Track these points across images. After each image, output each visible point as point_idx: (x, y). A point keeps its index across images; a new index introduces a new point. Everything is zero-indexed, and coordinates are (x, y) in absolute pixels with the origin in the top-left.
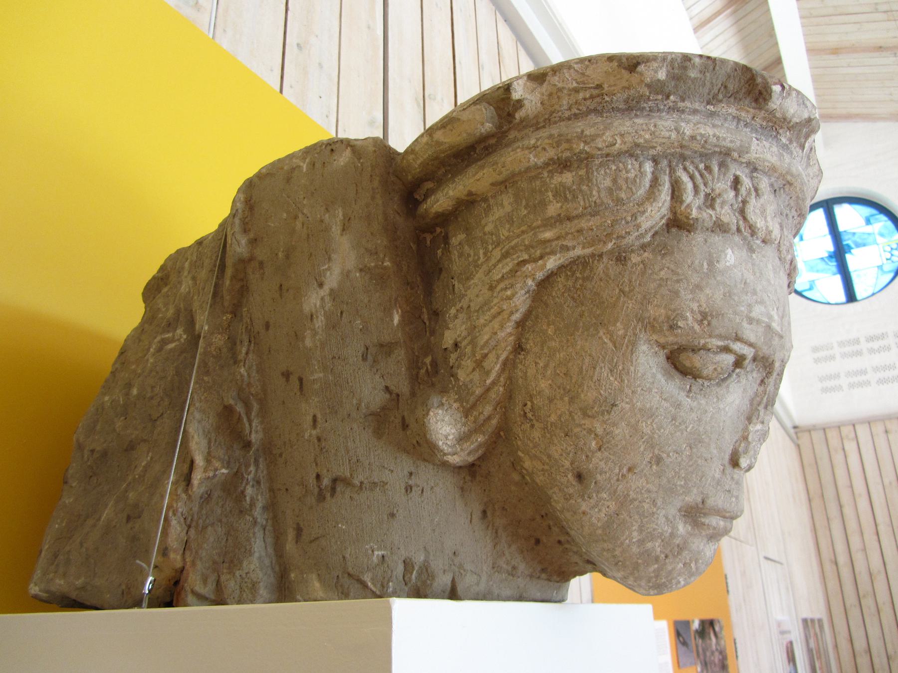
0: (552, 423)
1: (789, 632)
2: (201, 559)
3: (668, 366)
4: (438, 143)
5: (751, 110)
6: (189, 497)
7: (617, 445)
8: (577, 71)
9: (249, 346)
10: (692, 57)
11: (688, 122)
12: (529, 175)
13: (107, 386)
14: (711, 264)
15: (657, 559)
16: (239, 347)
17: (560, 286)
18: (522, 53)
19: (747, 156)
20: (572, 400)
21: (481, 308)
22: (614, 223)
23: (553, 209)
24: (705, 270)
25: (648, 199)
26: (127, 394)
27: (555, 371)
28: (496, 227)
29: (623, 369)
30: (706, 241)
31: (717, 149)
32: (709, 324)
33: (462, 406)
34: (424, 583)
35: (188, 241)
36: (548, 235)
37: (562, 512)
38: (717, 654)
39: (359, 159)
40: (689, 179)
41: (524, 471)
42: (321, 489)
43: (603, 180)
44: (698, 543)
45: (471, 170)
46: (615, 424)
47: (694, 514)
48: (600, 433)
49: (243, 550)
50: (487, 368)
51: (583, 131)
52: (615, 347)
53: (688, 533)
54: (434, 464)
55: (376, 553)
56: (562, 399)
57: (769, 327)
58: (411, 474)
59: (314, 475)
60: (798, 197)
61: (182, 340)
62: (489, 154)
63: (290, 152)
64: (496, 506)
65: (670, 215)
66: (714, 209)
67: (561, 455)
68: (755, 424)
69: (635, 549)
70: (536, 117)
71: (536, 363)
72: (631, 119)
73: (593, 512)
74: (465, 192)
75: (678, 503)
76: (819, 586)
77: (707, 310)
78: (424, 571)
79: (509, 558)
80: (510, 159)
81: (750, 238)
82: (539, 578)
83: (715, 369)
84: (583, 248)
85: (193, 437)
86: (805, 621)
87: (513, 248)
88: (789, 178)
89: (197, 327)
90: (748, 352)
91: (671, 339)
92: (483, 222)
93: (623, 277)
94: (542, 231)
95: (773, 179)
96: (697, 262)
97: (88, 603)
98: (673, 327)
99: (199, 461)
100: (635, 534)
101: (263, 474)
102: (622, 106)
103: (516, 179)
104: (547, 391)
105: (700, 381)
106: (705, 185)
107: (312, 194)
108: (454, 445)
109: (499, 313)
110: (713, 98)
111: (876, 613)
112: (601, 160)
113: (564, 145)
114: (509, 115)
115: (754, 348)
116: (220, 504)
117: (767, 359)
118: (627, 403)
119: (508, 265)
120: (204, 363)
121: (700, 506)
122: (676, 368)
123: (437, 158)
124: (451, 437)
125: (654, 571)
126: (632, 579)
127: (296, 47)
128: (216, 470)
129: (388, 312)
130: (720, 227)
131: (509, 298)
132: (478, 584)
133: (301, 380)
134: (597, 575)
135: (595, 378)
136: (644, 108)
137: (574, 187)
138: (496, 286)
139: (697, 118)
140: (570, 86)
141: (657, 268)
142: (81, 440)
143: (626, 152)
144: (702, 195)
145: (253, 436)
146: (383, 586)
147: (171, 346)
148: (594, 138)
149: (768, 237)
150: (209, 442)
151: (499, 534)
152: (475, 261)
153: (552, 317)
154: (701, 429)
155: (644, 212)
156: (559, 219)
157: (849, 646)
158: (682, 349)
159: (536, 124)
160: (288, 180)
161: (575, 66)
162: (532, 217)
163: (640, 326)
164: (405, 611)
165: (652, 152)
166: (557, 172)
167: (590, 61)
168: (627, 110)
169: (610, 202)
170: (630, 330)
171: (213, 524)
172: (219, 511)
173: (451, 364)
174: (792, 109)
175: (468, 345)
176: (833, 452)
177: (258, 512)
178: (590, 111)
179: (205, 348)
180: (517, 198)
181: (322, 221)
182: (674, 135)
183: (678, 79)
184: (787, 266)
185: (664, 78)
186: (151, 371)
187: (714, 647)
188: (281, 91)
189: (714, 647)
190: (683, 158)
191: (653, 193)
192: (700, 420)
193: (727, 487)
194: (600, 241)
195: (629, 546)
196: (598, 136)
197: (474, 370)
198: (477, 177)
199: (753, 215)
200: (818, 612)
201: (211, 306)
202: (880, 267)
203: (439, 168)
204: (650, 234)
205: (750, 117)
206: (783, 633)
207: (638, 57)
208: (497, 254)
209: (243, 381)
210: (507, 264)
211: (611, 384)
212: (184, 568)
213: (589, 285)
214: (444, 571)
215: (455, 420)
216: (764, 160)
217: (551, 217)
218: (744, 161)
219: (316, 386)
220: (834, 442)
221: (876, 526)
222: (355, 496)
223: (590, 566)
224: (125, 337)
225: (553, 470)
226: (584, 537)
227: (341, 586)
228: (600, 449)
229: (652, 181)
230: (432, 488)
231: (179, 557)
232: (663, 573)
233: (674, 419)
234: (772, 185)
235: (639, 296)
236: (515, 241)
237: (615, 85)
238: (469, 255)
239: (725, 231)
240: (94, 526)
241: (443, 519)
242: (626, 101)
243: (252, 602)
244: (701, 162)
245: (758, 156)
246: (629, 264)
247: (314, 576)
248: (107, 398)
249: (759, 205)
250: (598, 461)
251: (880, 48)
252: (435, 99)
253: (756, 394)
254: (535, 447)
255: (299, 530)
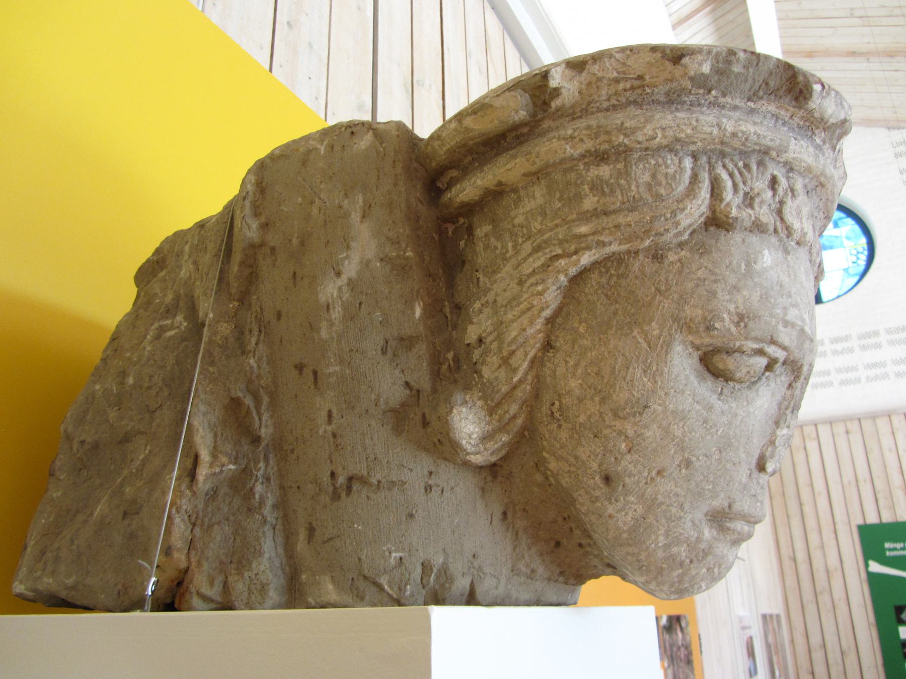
0: (580, 424)
1: (749, 628)
3: (700, 368)
4: (467, 130)
6: (194, 493)
8: (618, 61)
9: (259, 335)
10: (737, 51)
11: (729, 118)
12: (564, 166)
13: (98, 374)
14: (748, 264)
15: (681, 564)
16: (248, 337)
17: (594, 283)
20: (603, 401)
21: (509, 302)
22: (654, 219)
23: (589, 203)
24: (743, 271)
25: (688, 196)
26: (122, 383)
28: (527, 218)
29: (657, 370)
30: (744, 241)
31: (757, 148)
32: (746, 326)
33: (486, 403)
34: (442, 586)
35: (187, 223)
36: (583, 229)
37: (586, 515)
38: (682, 649)
39: (381, 144)
40: (728, 177)
41: (549, 473)
42: (335, 488)
44: (722, 548)
45: (502, 160)
46: (646, 427)
47: (720, 519)
48: (630, 435)
49: (252, 550)
51: (622, 123)
52: (650, 348)
54: (454, 464)
55: (394, 555)
56: (592, 399)
57: (802, 331)
58: (431, 473)
59: (329, 473)
60: (827, 199)
61: (182, 327)
62: (521, 143)
65: (708, 213)
66: (753, 208)
67: (589, 457)
68: (782, 429)
69: (660, 554)
70: (573, 106)
72: (672, 113)
73: (622, 514)
74: (495, 182)
76: (777, 581)
77: (744, 312)
78: (443, 573)
81: (785, 240)
82: (556, 581)
83: (748, 372)
84: (620, 244)
85: (198, 430)
86: (764, 617)
87: (545, 242)
88: (822, 179)
89: (201, 314)
90: (780, 355)
91: (707, 340)
92: (512, 214)
93: (659, 275)
94: (578, 226)
95: (807, 180)
96: (735, 262)
98: (709, 328)
99: (205, 456)
100: (661, 538)
101: (272, 470)
102: (662, 99)
103: (550, 170)
104: (577, 391)
105: (731, 383)
106: (744, 183)
109: (529, 309)
112: (640, 153)
113: (603, 137)
114: (545, 103)
116: (227, 502)
118: (660, 405)
119: (540, 260)
120: (209, 353)
121: (727, 510)
122: (709, 370)
123: (465, 145)
125: (678, 576)
126: (654, 583)
128: (223, 465)
129: (409, 304)
130: (758, 227)
131: (541, 294)
132: (497, 587)
133: (315, 373)
134: (617, 579)
135: (628, 378)
136: (685, 102)
137: (612, 181)
138: (526, 281)
139: (736, 115)
141: (694, 267)
144: (741, 194)
146: (400, 589)
147: (171, 333)
148: (634, 130)
149: (803, 239)
150: (215, 436)
153: (584, 315)
154: (731, 433)
155: (683, 210)
156: (596, 214)
158: (716, 351)
159: (573, 113)
160: (304, 163)
162: (566, 210)
163: (675, 326)
164: (441, 616)
165: (693, 148)
167: (631, 50)
168: (668, 103)
169: (649, 197)
170: (666, 330)
171: (219, 523)
172: (226, 509)
173: (474, 361)
174: (829, 109)
175: (494, 341)
178: (629, 103)
179: (210, 337)
180: (550, 189)
181: (340, 207)
182: (715, 131)
183: (722, 74)
184: (816, 269)
185: (708, 71)
186: (149, 359)
188: (271, 70)
190: (723, 155)
191: (693, 190)
192: (730, 423)
193: (753, 492)
194: (637, 237)
195: (654, 550)
196: (638, 128)
197: (500, 366)
198: (509, 166)
199: (790, 217)
200: (775, 607)
202: (846, 270)
203: (466, 156)
204: (688, 232)
205: (789, 115)
206: (744, 628)
207: (683, 49)
208: (528, 247)
209: (252, 372)
210: (539, 259)
211: (644, 385)
212: (188, 568)
213: (623, 282)
214: (463, 574)
215: (479, 418)
216: (801, 161)
217: (587, 211)
218: (782, 160)
219: (333, 380)
222: (372, 495)
223: (609, 570)
224: (116, 323)
225: (579, 472)
227: (357, 588)
228: (629, 451)
229: (691, 178)
231: (183, 557)
233: (705, 422)
234: (805, 186)
235: (676, 296)
237: (657, 77)
238: (496, 248)
239: (763, 232)
240: (86, 521)
241: (459, 522)
242: (667, 94)
244: (741, 160)
245: (795, 155)
246: (666, 262)
247: (327, 578)
248: (98, 387)
250: (627, 463)
253: (784, 398)
254: (562, 448)
255: (311, 530)
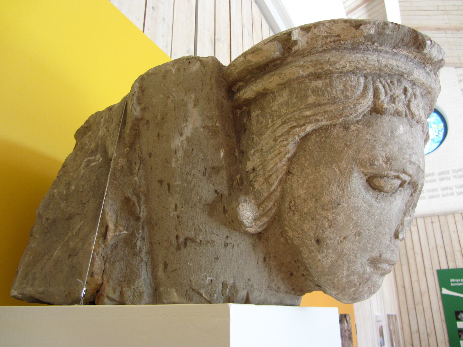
0: (305, 213)
1: (381, 321)
2: (112, 279)
3: (366, 184)
4: (249, 61)
5: (415, 53)
6: (106, 245)
8: (327, 27)
9: (140, 165)
11: (384, 57)
12: (298, 81)
13: (56, 184)
15: (355, 285)
16: (134, 166)
17: (313, 141)
18: (264, 20)
19: (411, 77)
20: (317, 201)
21: (269, 150)
22: (344, 108)
23: (311, 99)
25: (362, 97)
26: (68, 189)
27: (308, 185)
28: (279, 107)
31: (397, 73)
32: (390, 164)
34: (233, 295)
35: (102, 108)
36: (308, 113)
38: (347, 332)
42: (178, 244)
43: (338, 85)
44: (376, 278)
45: (266, 77)
46: (338, 214)
47: (375, 262)
49: (135, 275)
50: (271, 182)
51: (329, 59)
52: (341, 174)
53: (372, 272)
54: (239, 232)
55: (208, 278)
56: (311, 200)
57: (419, 167)
58: (227, 237)
59: (175, 236)
60: (432, 100)
61: (100, 161)
63: (166, 62)
64: (271, 255)
65: (372, 106)
66: (395, 104)
67: (309, 229)
68: (407, 217)
69: (344, 280)
70: (304, 50)
71: (298, 181)
72: (354, 54)
73: (325, 259)
74: (263, 88)
75: (368, 256)
77: (390, 156)
78: (233, 288)
79: (276, 283)
80: (289, 72)
81: (411, 120)
82: (290, 293)
83: (391, 187)
84: (327, 121)
85: (108, 213)
86: (388, 316)
87: (288, 119)
88: (430, 90)
89: (110, 154)
90: (407, 179)
91: (370, 171)
92: (271, 105)
93: (347, 137)
94: (305, 111)
96: (385, 131)
99: (111, 226)
100: (345, 272)
101: (146, 234)
104: (303, 196)
105: (382, 193)
106: (391, 91)
108: (252, 222)
109: (279, 154)
111: (423, 312)
112: (337, 75)
116: (123, 250)
118: (346, 203)
119: (285, 128)
120: (114, 174)
121: (379, 258)
122: (371, 186)
123: (247, 69)
124: (250, 218)
126: (341, 295)
127: (151, 8)
128: (121, 231)
130: (397, 113)
131: (285, 146)
132: (260, 296)
133: (169, 185)
134: (321, 293)
135: (330, 189)
136: (361, 48)
137: (323, 88)
139: (387, 56)
141: (365, 133)
142: (41, 212)
143: (351, 71)
144: (389, 96)
145: (141, 214)
147: (93, 164)
148: (335, 63)
149: (420, 120)
150: (117, 216)
151: (272, 270)
153: (308, 157)
155: (360, 103)
156: (314, 105)
157: (409, 329)
158: (375, 176)
160: (164, 77)
164: (235, 309)
165: (364, 72)
166: (314, 80)
167: (334, 22)
168: (352, 49)
169: (342, 97)
172: (122, 254)
175: (261, 170)
177: (143, 255)
178: (333, 49)
180: (291, 92)
181: (183, 100)
182: (376, 64)
184: (425, 135)
186: (82, 177)
188: (143, 31)
191: (365, 94)
192: (381, 214)
193: (392, 249)
194: (336, 117)
196: (337, 62)
197: (264, 183)
198: (270, 80)
199: (413, 109)
200: (394, 311)
201: (118, 144)
204: (362, 115)
208: (279, 122)
209: (136, 184)
211: (338, 193)
212: (102, 283)
213: (328, 141)
215: (253, 209)
217: (310, 104)
218: (409, 79)
219: (178, 188)
222: (198, 248)
223: (318, 288)
225: (304, 237)
226: (318, 273)
227: (189, 295)
228: (330, 227)
229: (364, 87)
230: (238, 245)
233: (369, 212)
235: (355, 148)
237: (347, 36)
238: (262, 122)
240: (49, 259)
241: (241, 261)
242: (352, 45)
243: (140, 303)
246: (350, 130)
247: (174, 290)
248: (55, 191)
250: (328, 233)
253: (408, 201)
254: (295, 225)
255: (166, 265)
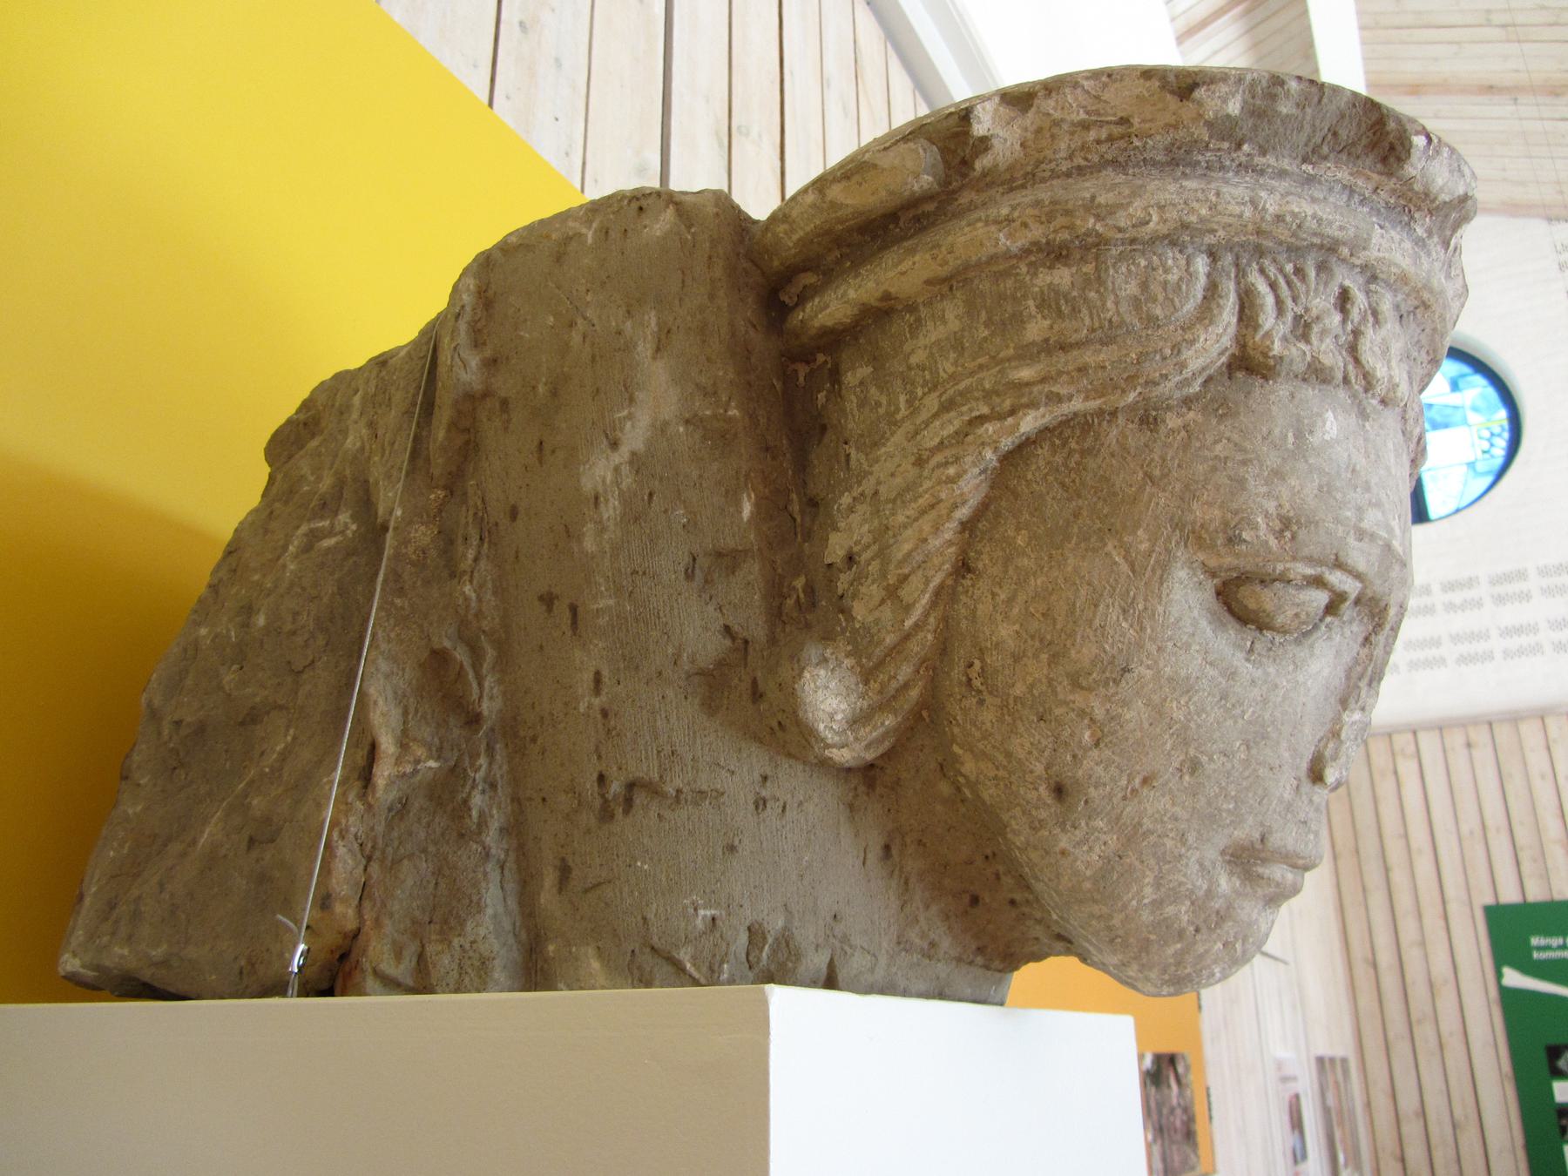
0: (1016, 699)
1: (1294, 1079)
2: (391, 915)
4: (834, 205)
5: (1375, 176)
6: (370, 807)
7: (1127, 739)
9: (480, 546)
11: (1271, 191)
12: (995, 268)
14: (1299, 435)
15: (1181, 934)
16: (461, 549)
17: (1042, 463)
19: (1362, 254)
20: (1054, 659)
23: (1036, 329)
24: (1290, 446)
25: (1200, 319)
26: (246, 625)
28: (931, 355)
30: (1292, 396)
31: (1317, 241)
32: (1293, 538)
33: (859, 663)
35: (356, 359)
36: (1026, 373)
38: (1178, 1112)
39: (689, 227)
40: (1268, 289)
41: (961, 779)
42: (606, 801)
44: (1249, 909)
45: (890, 257)
46: (1125, 703)
47: (1247, 859)
51: (1093, 198)
52: (1134, 571)
54: (804, 763)
55: (702, 912)
57: (1388, 547)
58: (765, 778)
59: (595, 776)
60: (1435, 330)
62: (923, 229)
65: (1234, 350)
66: (1308, 342)
67: (1030, 753)
68: (1352, 711)
69: (1146, 916)
70: (1011, 168)
71: (994, 595)
72: (1175, 180)
73: (1083, 849)
74: (878, 294)
75: (1221, 840)
77: (1291, 514)
79: (925, 928)
81: (1362, 395)
82: (971, 963)
83: (1297, 615)
84: (1087, 398)
85: (375, 703)
86: (1320, 1061)
87: (961, 394)
88: (1426, 295)
90: (1351, 586)
91: (1229, 560)
92: (907, 348)
94: (1016, 368)
95: (1400, 297)
96: (1277, 431)
97: (172, 989)
98: (1233, 540)
99: (387, 744)
100: (1148, 890)
101: (501, 770)
104: (1010, 641)
105: (1268, 634)
107: (603, 284)
109: (932, 506)
110: (1313, 151)
113: (1060, 221)
115: (1362, 581)
117: (1377, 605)
118: (1148, 667)
121: (1258, 846)
122: (1230, 610)
123: (828, 232)
126: (1135, 967)
128: (417, 762)
129: (733, 497)
130: (1317, 373)
132: (872, 970)
133: (574, 609)
134: (1073, 961)
135: (1097, 622)
136: (1198, 162)
137: (1075, 293)
139: (1284, 185)
140: (1075, 117)
141: (1210, 439)
142: (157, 702)
143: (1165, 237)
144: (1289, 317)
148: (1112, 210)
150: (405, 713)
151: (911, 886)
152: (892, 415)
154: (1267, 716)
155: (1193, 342)
156: (1048, 347)
158: (1244, 579)
160: (559, 258)
161: (1085, 83)
164: (789, 1006)
165: (1209, 239)
166: (1044, 265)
167: (1109, 76)
168: (1169, 164)
170: (1160, 542)
171: (411, 856)
172: (422, 835)
173: (840, 592)
174: (1439, 177)
175: (873, 559)
176: (1376, 777)
177: (491, 837)
180: (971, 308)
182: (1248, 212)
183: (1259, 116)
184: (1413, 446)
187: (1175, 1101)
188: (491, 104)
189: (1175, 1101)
190: (1260, 252)
192: (1265, 701)
193: (1302, 816)
197: (883, 602)
198: (902, 268)
200: (1339, 1045)
204: (1200, 380)
206: (1285, 1080)
208: (932, 403)
210: (950, 422)
211: (1123, 635)
213: (1091, 463)
215: (847, 688)
216: (1391, 263)
217: (1033, 343)
218: (1358, 262)
219: (603, 621)
220: (1380, 758)
221: (1444, 902)
222: (667, 814)
223: (1059, 945)
224: (235, 525)
225: (1013, 779)
228: (1097, 744)
229: (1206, 290)
231: (351, 912)
232: (1189, 959)
234: (1397, 307)
235: (1178, 486)
236: (967, 382)
237: (1151, 120)
238: (878, 404)
240: (184, 854)
241: (813, 854)
242: (1168, 150)
244: (1289, 261)
246: (1163, 430)
247: (591, 951)
248: (203, 631)
249: (1379, 339)
251: (1490, 89)
252: (747, 135)
253: (1356, 661)
254: (984, 738)
255: (565, 871)
